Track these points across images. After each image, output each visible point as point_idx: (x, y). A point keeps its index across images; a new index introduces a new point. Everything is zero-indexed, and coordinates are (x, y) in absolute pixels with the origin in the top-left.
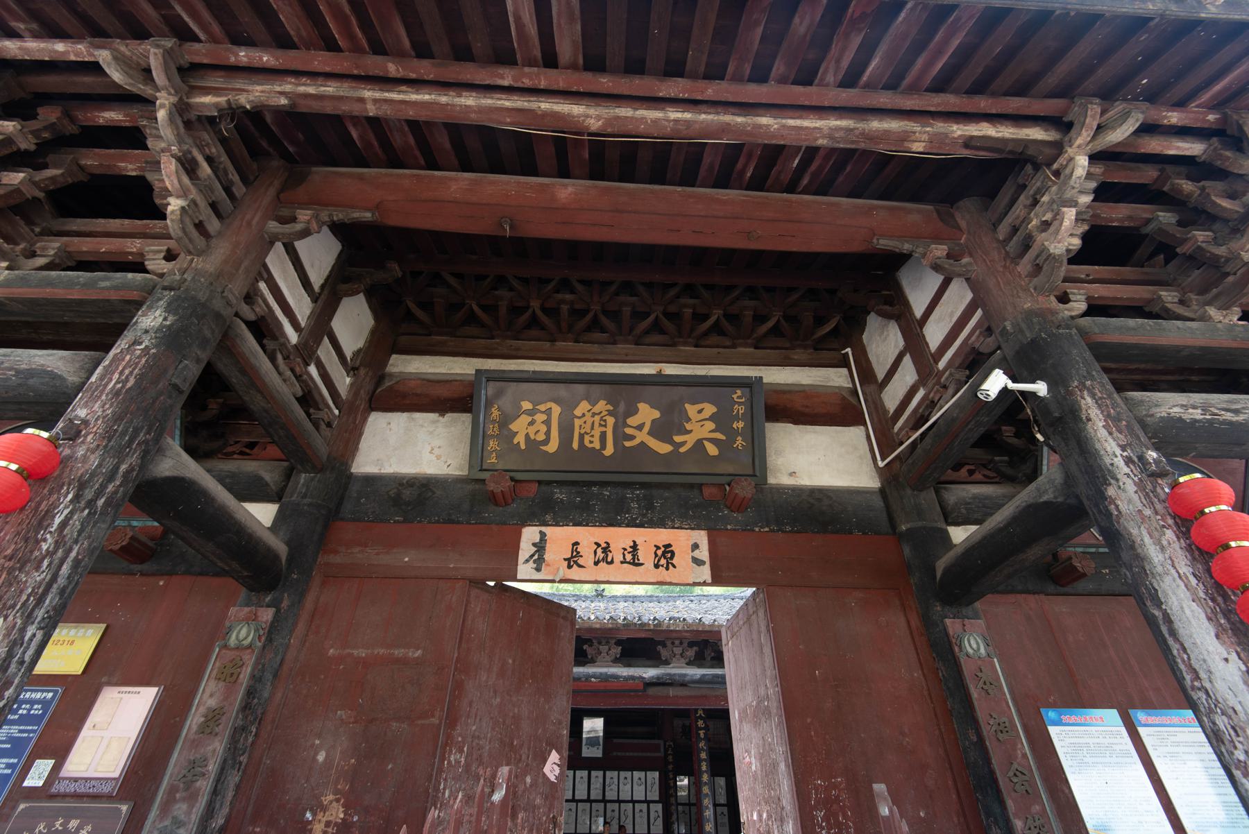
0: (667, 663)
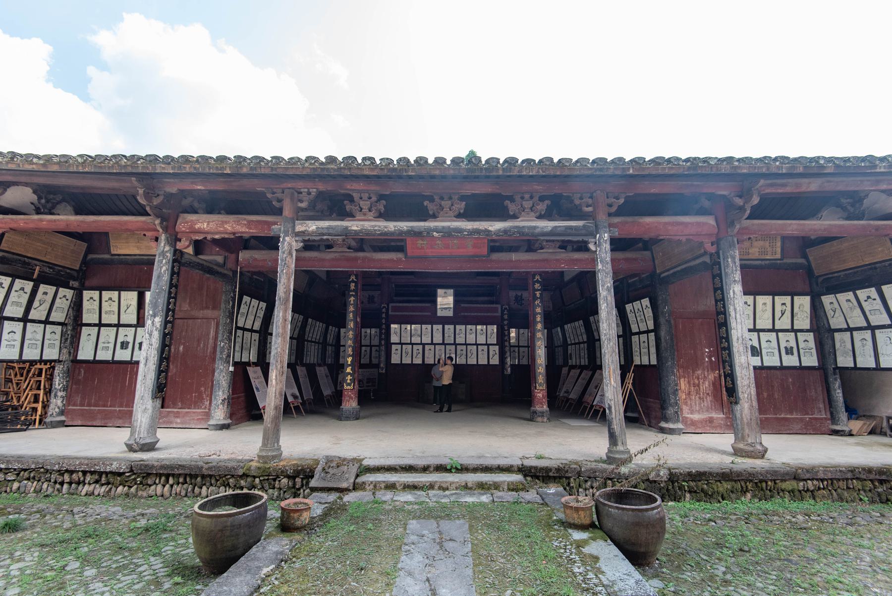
0: (515, 217)
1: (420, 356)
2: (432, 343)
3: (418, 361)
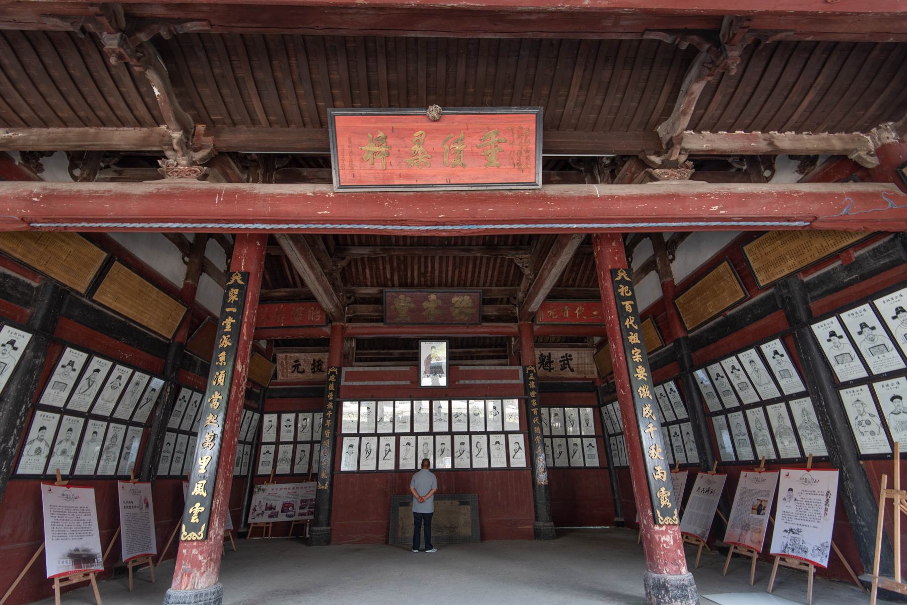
1: (392, 455)
2: (412, 433)
3: (387, 465)
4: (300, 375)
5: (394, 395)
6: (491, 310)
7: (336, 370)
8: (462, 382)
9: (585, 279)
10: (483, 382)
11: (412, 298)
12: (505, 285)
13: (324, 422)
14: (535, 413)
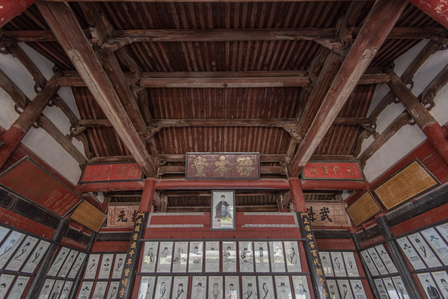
2: (204, 273)
4: (123, 223)
5: (189, 236)
6: (266, 170)
7: (143, 214)
8: (246, 226)
9: (335, 148)
10: (265, 225)
11: (206, 158)
12: (275, 153)
13: (127, 261)
14: (315, 254)
